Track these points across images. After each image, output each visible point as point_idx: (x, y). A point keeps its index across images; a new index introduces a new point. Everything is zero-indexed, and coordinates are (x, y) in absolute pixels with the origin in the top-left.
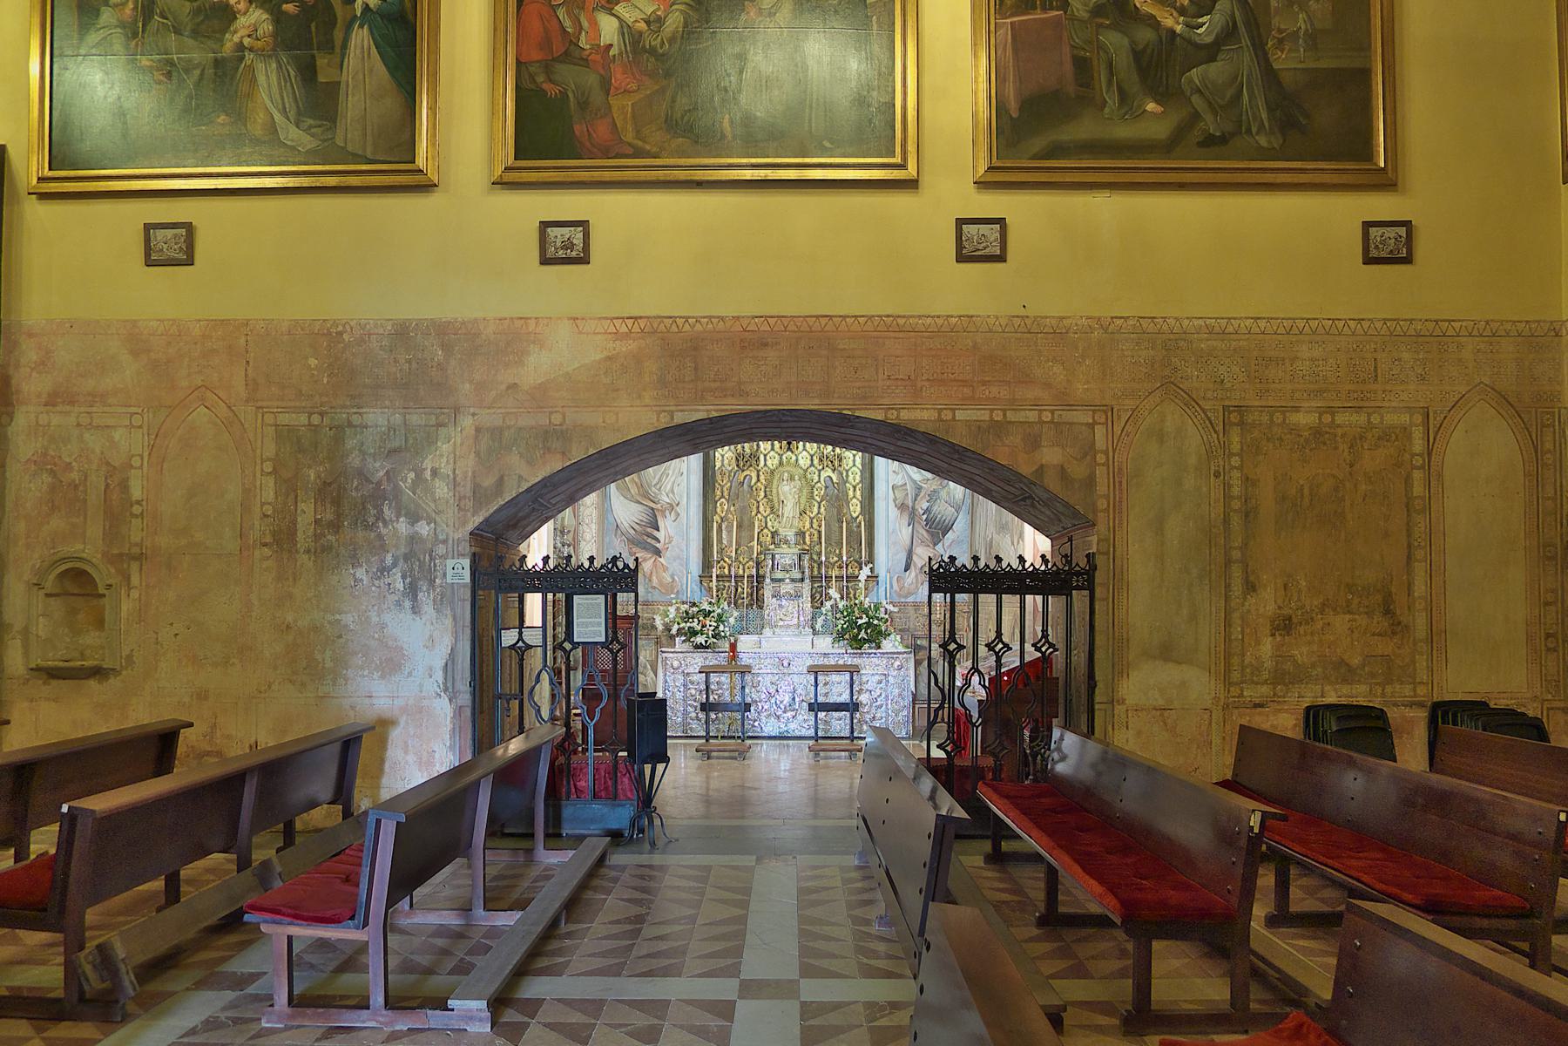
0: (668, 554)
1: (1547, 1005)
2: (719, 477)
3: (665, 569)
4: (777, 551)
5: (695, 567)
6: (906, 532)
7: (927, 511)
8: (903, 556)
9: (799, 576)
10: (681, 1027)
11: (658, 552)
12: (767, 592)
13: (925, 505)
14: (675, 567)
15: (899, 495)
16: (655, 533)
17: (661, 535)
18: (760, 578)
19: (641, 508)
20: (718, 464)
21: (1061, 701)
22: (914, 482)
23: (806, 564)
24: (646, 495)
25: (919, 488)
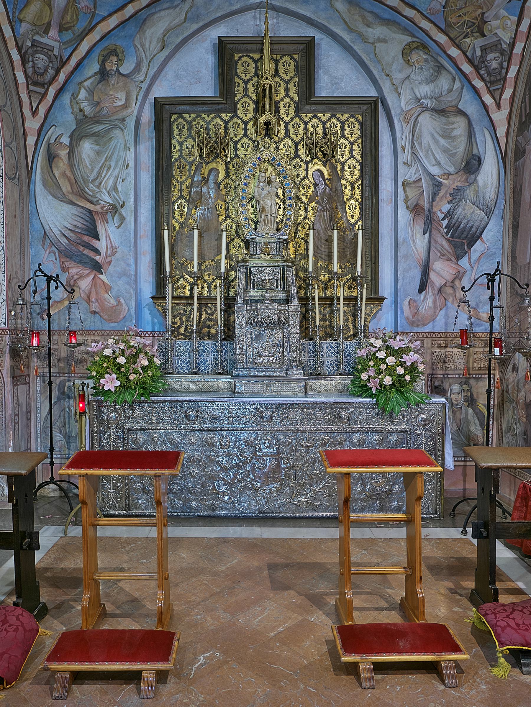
0: (111, 269)
1: (525, 684)
2: (176, 173)
3: (107, 288)
4: (253, 262)
5: (147, 289)
6: (420, 242)
7: (449, 214)
8: (416, 274)
9: (282, 296)
10: (98, 84)
11: (97, 267)
12: (240, 319)
13: (446, 207)
14: (120, 285)
15: (412, 193)
16: (95, 243)
17: (101, 245)
18: (229, 303)
19: (74, 210)
20: (176, 155)
21: (382, 516)
22: (432, 177)
23: (292, 280)
24: (82, 194)
25: (438, 186)
